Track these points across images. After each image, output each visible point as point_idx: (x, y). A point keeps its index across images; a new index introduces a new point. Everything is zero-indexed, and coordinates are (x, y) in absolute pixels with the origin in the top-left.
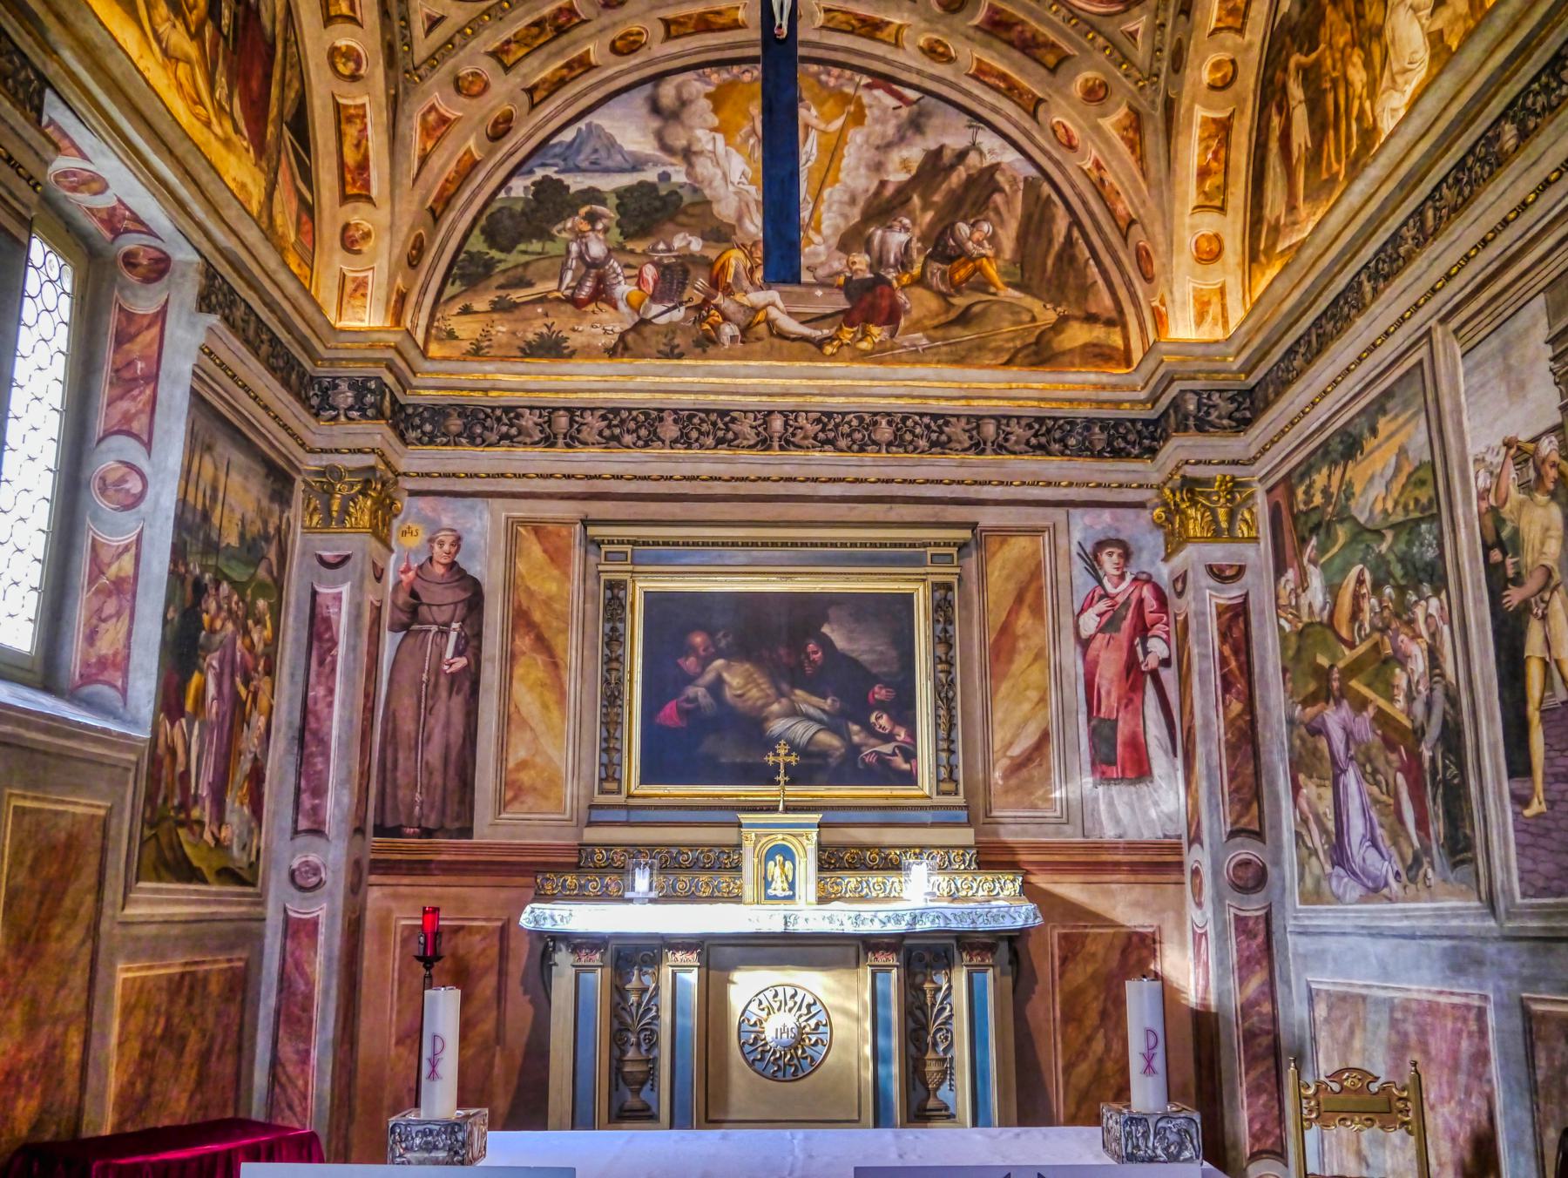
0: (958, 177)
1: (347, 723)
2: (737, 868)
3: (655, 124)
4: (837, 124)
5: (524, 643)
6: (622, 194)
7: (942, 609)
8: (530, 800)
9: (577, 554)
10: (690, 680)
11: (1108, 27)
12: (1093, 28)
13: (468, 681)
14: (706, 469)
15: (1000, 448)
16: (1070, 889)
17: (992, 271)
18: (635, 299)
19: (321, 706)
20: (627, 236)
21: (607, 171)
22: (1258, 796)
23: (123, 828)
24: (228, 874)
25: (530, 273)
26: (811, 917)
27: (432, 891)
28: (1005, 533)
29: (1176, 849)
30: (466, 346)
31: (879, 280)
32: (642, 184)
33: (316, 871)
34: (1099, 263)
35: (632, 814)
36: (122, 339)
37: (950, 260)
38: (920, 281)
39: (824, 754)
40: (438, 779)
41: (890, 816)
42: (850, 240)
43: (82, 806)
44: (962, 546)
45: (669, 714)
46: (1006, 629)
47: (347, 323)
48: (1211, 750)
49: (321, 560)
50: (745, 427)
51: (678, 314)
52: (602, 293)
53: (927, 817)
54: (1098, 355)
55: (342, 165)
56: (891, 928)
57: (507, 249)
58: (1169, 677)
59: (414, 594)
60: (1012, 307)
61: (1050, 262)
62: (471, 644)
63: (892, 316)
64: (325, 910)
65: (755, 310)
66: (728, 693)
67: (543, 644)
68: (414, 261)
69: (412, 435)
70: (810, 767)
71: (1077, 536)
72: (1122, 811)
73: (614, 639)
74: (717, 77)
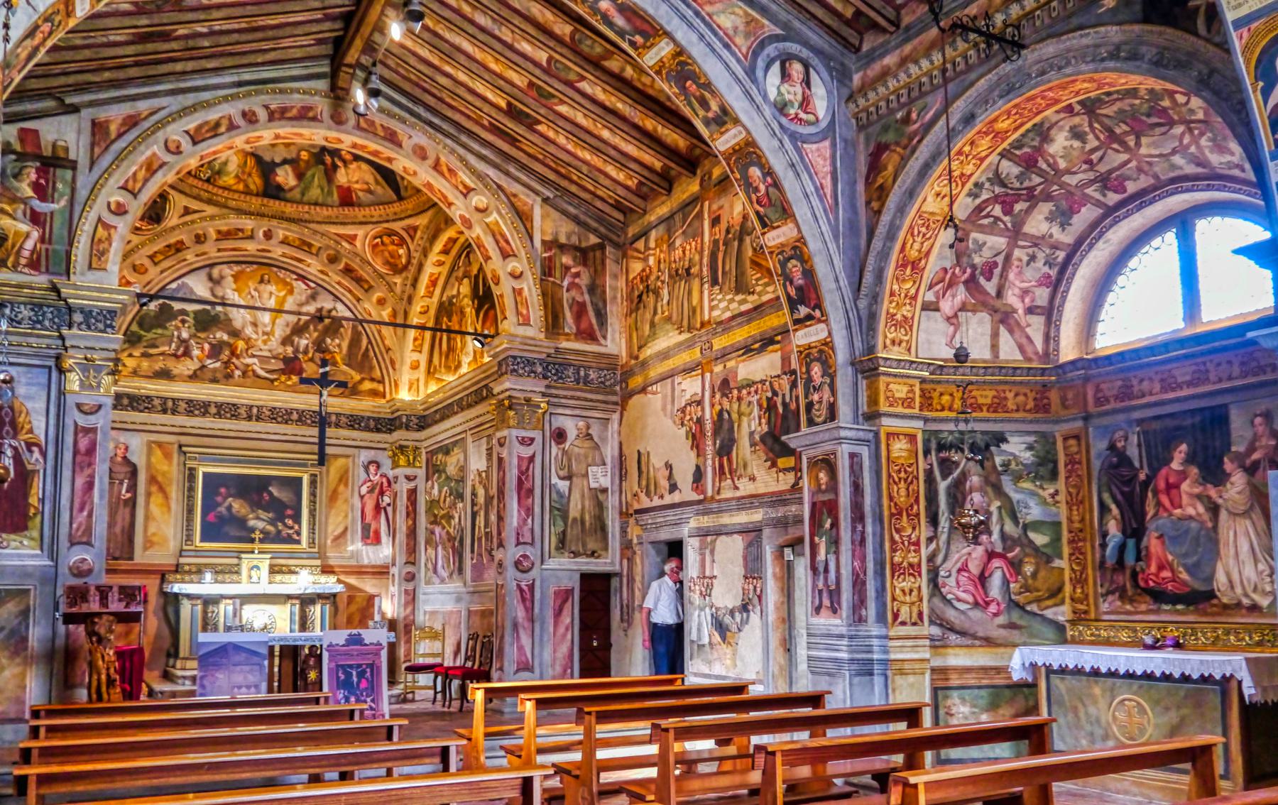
3: (210, 285)
4: (283, 294)
5: (154, 489)
6: (196, 313)
7: (313, 483)
8: (156, 547)
9: (175, 456)
10: (219, 505)
11: (388, 278)
13: (132, 503)
14: (227, 427)
17: (338, 358)
22: (414, 551)
25: (158, 343)
29: (387, 567)
31: (296, 358)
38: (311, 360)
40: (119, 538)
42: (286, 341)
50: (242, 411)
51: (218, 365)
52: (187, 353)
54: (374, 393)
57: (148, 331)
58: (390, 510)
62: (133, 488)
65: (248, 365)
66: (234, 510)
67: (162, 489)
70: (267, 539)
73: (191, 489)
74: (236, 268)
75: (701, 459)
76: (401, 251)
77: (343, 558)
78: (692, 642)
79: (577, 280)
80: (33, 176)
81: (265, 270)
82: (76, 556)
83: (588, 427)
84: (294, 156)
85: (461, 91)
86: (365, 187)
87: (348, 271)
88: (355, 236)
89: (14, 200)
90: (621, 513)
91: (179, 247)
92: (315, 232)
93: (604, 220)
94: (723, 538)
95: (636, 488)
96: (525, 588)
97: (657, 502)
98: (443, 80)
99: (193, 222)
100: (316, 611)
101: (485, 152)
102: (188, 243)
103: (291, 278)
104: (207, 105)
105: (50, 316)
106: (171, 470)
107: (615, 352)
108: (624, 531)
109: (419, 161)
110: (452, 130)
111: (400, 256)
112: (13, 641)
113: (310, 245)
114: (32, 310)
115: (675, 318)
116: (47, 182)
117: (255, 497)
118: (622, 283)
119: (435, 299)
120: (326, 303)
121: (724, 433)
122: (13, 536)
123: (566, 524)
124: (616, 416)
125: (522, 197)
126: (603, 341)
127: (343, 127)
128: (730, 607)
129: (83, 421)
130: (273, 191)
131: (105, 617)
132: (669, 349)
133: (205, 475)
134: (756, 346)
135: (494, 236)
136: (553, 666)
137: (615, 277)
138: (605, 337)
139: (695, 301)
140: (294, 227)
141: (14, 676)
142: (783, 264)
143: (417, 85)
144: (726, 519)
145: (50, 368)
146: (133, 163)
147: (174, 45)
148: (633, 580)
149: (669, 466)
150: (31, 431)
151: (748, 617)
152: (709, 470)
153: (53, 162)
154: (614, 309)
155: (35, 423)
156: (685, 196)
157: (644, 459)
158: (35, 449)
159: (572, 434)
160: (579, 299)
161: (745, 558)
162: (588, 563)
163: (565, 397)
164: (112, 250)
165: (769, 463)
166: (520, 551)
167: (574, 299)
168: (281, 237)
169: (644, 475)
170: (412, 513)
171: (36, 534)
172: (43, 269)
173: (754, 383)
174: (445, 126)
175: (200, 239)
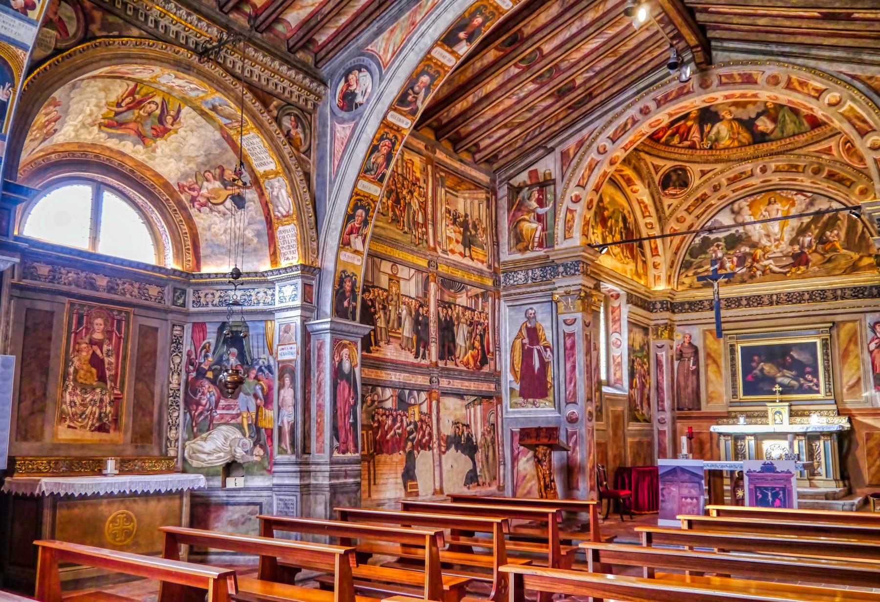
1: (668, 385)
2: (767, 417)
3: (733, 216)
4: (786, 208)
5: (710, 362)
6: (726, 238)
7: (825, 345)
8: (715, 401)
10: (755, 368)
13: (697, 372)
14: (755, 312)
15: (843, 298)
17: (838, 245)
20: (728, 250)
23: (626, 412)
24: (645, 420)
26: (786, 427)
27: (691, 423)
28: (844, 322)
31: (803, 253)
35: (741, 403)
36: (613, 313)
38: (815, 251)
39: (793, 387)
40: (691, 397)
41: (812, 402)
42: (792, 242)
43: (620, 408)
44: (831, 328)
45: (749, 378)
50: (765, 299)
51: (744, 270)
55: (651, 248)
57: (696, 258)
60: (844, 255)
61: (857, 239)
62: (696, 362)
64: (667, 428)
65: (766, 266)
66: (765, 372)
67: (715, 362)
68: (671, 267)
69: (676, 310)
70: (787, 390)
71: (868, 321)
73: (733, 359)
74: (750, 200)
77: (859, 403)
80: (537, 195)
81: (771, 194)
82: (570, 410)
84: (763, 108)
85: (780, 22)
87: (831, 176)
88: (830, 147)
91: (704, 198)
92: (799, 156)
98: (762, 21)
99: (709, 179)
100: (820, 445)
101: (834, 54)
103: (791, 195)
104: (616, 117)
109: (773, 87)
113: (797, 167)
117: (780, 360)
120: (823, 204)
122: (541, 400)
127: (709, 89)
129: (568, 329)
130: (760, 138)
131: (541, 447)
133: (742, 348)
147: (579, 91)
150: (545, 340)
153: (544, 184)
155: (547, 334)
171: (551, 398)
174: (794, 50)
175: (716, 189)
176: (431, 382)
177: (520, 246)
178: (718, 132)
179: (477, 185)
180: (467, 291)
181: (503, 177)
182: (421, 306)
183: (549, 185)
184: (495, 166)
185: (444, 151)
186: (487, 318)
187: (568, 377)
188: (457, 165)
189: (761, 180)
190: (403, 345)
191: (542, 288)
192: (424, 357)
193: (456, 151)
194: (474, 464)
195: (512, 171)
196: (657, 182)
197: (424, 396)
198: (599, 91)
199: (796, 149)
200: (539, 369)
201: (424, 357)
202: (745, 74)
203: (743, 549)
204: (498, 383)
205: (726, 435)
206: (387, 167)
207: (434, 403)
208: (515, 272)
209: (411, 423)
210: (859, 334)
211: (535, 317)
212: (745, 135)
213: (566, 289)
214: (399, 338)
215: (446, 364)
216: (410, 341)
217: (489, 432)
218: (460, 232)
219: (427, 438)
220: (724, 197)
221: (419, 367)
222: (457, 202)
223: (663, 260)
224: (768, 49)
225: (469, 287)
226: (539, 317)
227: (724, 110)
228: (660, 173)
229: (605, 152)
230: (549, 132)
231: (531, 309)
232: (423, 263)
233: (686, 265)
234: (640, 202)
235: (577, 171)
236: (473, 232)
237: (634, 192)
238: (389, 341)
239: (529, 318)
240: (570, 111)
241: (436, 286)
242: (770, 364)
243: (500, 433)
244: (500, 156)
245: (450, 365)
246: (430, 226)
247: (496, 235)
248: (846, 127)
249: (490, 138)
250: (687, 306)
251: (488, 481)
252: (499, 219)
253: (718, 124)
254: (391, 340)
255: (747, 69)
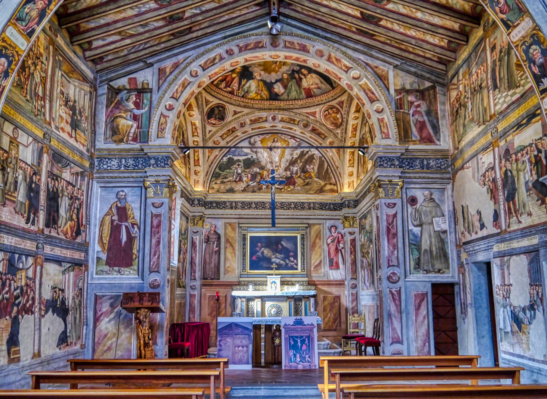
0: (307, 156)
1: (199, 260)
2: (266, 285)
5: (228, 245)
6: (244, 160)
7: (303, 238)
8: (230, 273)
9: (237, 229)
10: (258, 252)
11: (334, 131)
12: (331, 131)
13: (218, 252)
14: (260, 213)
15: (314, 209)
16: (325, 288)
17: (313, 175)
18: (247, 181)
19: (194, 258)
20: (245, 169)
21: (241, 156)
22: (356, 272)
25: (227, 176)
28: (314, 224)
29: (344, 281)
30: (216, 190)
31: (292, 177)
32: (248, 158)
33: (195, 286)
34: (333, 173)
35: (248, 276)
37: (305, 172)
38: (299, 177)
39: (281, 265)
40: (213, 269)
41: (293, 275)
42: (286, 169)
44: (306, 227)
45: (254, 258)
46: (314, 242)
47: (196, 189)
48: (349, 264)
49: (193, 232)
51: (255, 184)
52: (241, 180)
53: (300, 276)
54: (332, 191)
55: (195, 160)
56: (292, 295)
57: (223, 171)
58: (343, 250)
59: (208, 236)
60: (316, 182)
62: (219, 245)
63: (294, 184)
66: (265, 254)
67: (231, 245)
69: (207, 207)
70: (279, 267)
72: (334, 275)
73: (244, 244)
74: (262, 137)
75: (497, 205)
76: (338, 116)
78: (501, 329)
79: (418, 109)
80: (134, 99)
81: (276, 136)
82: (154, 277)
83: (431, 194)
84: (280, 77)
85: (335, 13)
86: (316, 86)
87: (314, 130)
88: (316, 112)
89: (126, 111)
90: (457, 245)
91: (233, 130)
92: (296, 113)
93: (433, 71)
94: (514, 257)
95: (463, 229)
96: (395, 293)
97: (474, 236)
99: (239, 117)
101: (357, 47)
102: (237, 128)
103: (287, 138)
104: (207, 51)
105: (141, 162)
106: (235, 236)
107: (447, 148)
108: (459, 257)
109: (320, 58)
110: (338, 39)
111: (338, 119)
112: (126, 320)
113: (294, 120)
114: (134, 160)
115: (475, 119)
116: (140, 100)
117: (274, 247)
118: (448, 107)
119: (358, 138)
121: (509, 186)
122: (126, 269)
123: (420, 253)
124: (449, 187)
125: (381, 67)
126: (438, 142)
127: (278, 48)
128: (523, 306)
129: (155, 211)
130: (274, 97)
131: (143, 310)
132: (474, 138)
133: (251, 237)
134: (525, 121)
135: (365, 91)
136: (416, 341)
137: (444, 104)
138: (439, 140)
139: (485, 104)
140: (286, 113)
141: (127, 338)
142: (526, 52)
143: (315, 18)
144: (516, 245)
145: (141, 187)
146: (176, 85)
147: (186, 22)
148: (466, 287)
149: (479, 213)
150: (133, 218)
151: (535, 314)
152: (502, 212)
154: (444, 122)
155: (135, 214)
156: (475, 41)
157: (465, 210)
158: (135, 226)
159: (420, 199)
160: (420, 119)
161: (529, 271)
162: (435, 277)
163: (415, 178)
164: (167, 127)
165: (540, 202)
166: (390, 271)
167: (417, 120)
168: (280, 118)
169: (466, 220)
170: (353, 251)
171: (136, 268)
172: (138, 141)
173: (525, 147)
174: (333, 37)
175: (242, 125)
176: (37, 248)
177: (116, 138)
178: (250, 87)
179: (85, 79)
180: (71, 168)
181: (104, 78)
182: (35, 174)
183: (147, 92)
184: (99, 67)
185: (63, 38)
186: (82, 195)
187: (153, 251)
188: (72, 55)
189: (271, 125)
190: (17, 209)
191: (134, 175)
192: (33, 224)
193: (72, 43)
194: (66, 325)
195: (113, 75)
196: (205, 113)
197: (31, 260)
198: (197, 28)
199: (295, 109)
200: (125, 242)
201: (33, 224)
202: (302, 44)
203: (308, 387)
204: (87, 252)
205: (241, 297)
206: (38, 23)
207: (38, 268)
208: (109, 159)
209: (18, 287)
210: (322, 233)
211: (125, 199)
212: (266, 93)
213: (157, 178)
214: (14, 202)
215: (50, 232)
216: (23, 206)
217: (78, 296)
218: (69, 114)
219: (30, 302)
220: (246, 132)
221: (29, 232)
222: (69, 87)
223: (202, 169)
224: (317, 32)
225: (72, 165)
226: (129, 199)
227: (257, 72)
228: (209, 106)
229: (197, 76)
230: (151, 49)
231: (123, 191)
232: (40, 134)
233: (216, 176)
234: (193, 124)
235: (172, 85)
236: (79, 118)
237: (191, 116)
238: (5, 204)
239: (119, 199)
240: (172, 37)
241: (48, 157)
242: (268, 249)
243: (85, 297)
244: (104, 60)
245: (53, 234)
246: (47, 102)
247: (94, 124)
248: (362, 95)
249: (103, 40)
250: (214, 205)
251: (74, 341)
252: (97, 112)
253: (251, 81)
254: (7, 202)
255: (304, 42)
